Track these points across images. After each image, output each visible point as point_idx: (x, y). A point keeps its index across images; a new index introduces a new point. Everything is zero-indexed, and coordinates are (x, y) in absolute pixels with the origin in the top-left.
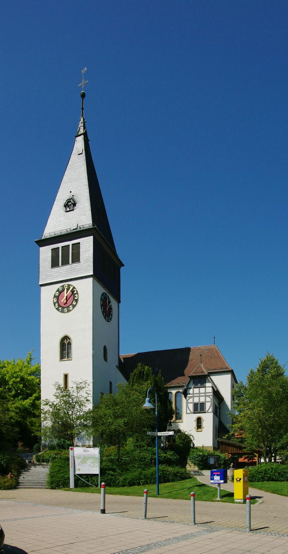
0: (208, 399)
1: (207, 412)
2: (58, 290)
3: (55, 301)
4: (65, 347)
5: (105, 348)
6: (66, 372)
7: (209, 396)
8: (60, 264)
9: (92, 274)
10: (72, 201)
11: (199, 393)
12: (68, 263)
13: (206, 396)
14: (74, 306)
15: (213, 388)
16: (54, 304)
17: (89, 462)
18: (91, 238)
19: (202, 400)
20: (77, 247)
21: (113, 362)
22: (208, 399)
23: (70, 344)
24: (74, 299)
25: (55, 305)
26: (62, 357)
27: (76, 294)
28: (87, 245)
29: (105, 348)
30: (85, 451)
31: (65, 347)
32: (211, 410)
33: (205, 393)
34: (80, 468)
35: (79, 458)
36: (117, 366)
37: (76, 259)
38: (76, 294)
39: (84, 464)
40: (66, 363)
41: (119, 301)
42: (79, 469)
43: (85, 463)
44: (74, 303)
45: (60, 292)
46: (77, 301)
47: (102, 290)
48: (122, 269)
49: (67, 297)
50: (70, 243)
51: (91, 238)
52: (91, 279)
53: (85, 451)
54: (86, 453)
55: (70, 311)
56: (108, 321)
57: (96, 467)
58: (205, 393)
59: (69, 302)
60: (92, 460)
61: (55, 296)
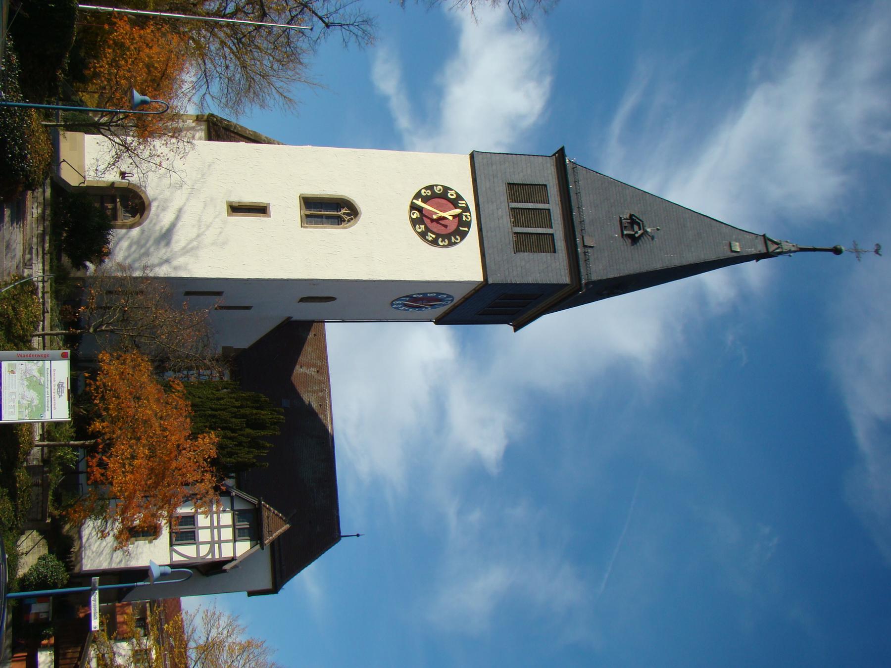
0: (204, 550)
1: (172, 550)
2: (459, 197)
3: (437, 190)
4: (328, 210)
5: (331, 299)
6: (272, 210)
7: (212, 550)
8: (514, 205)
9: (490, 281)
10: (640, 232)
11: (219, 527)
12: (516, 223)
13: (212, 543)
14: (423, 235)
15: (233, 559)
16: (430, 188)
17: (32, 394)
18: (565, 279)
19: (204, 535)
20: (545, 244)
21: (303, 312)
22: (204, 550)
23: (339, 221)
24: (438, 236)
25: (427, 188)
26: (309, 202)
27: (450, 240)
28: (550, 268)
29: (331, 299)
30: (60, 386)
31: (328, 210)
32: (177, 558)
33: (220, 542)
34: (18, 374)
35: (41, 371)
36: (289, 318)
37: (523, 243)
38: (450, 240)
39: (26, 383)
40: (295, 211)
41: (438, 322)
42: (13, 372)
43: (28, 387)
44: (430, 237)
45: (455, 202)
46: (434, 243)
47: (458, 296)
48: (507, 328)
49: (444, 218)
50: (558, 230)
51: (565, 279)
52: (480, 278)
53: (60, 386)
54: (55, 388)
55: (414, 226)
56: (392, 304)
57: (20, 413)
58: (220, 542)
59: (434, 227)
60: (36, 402)
61: (446, 189)
